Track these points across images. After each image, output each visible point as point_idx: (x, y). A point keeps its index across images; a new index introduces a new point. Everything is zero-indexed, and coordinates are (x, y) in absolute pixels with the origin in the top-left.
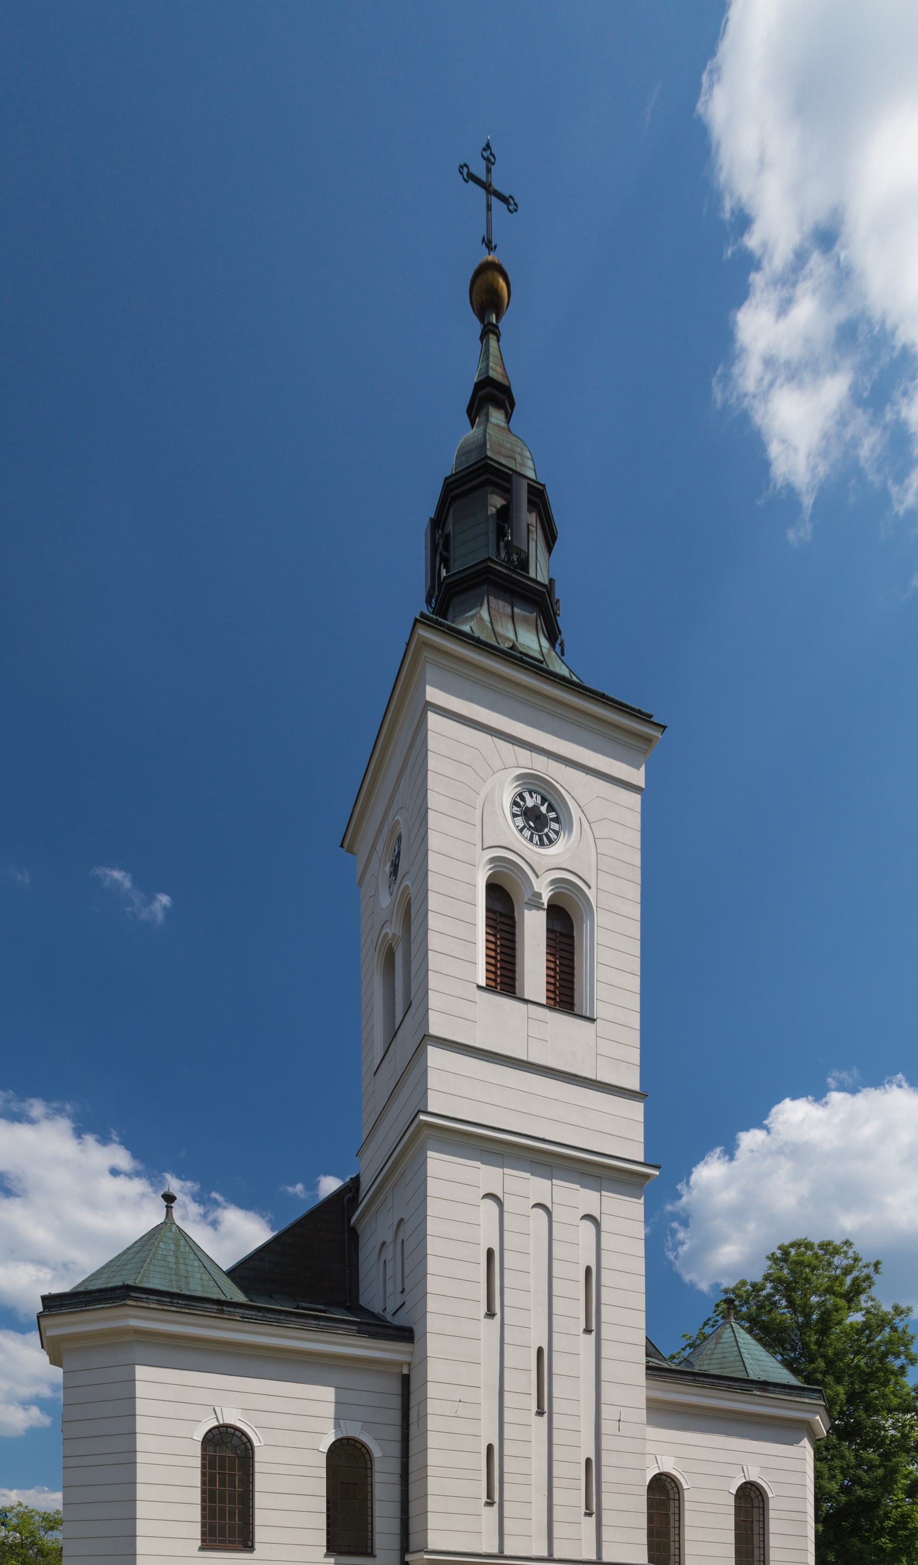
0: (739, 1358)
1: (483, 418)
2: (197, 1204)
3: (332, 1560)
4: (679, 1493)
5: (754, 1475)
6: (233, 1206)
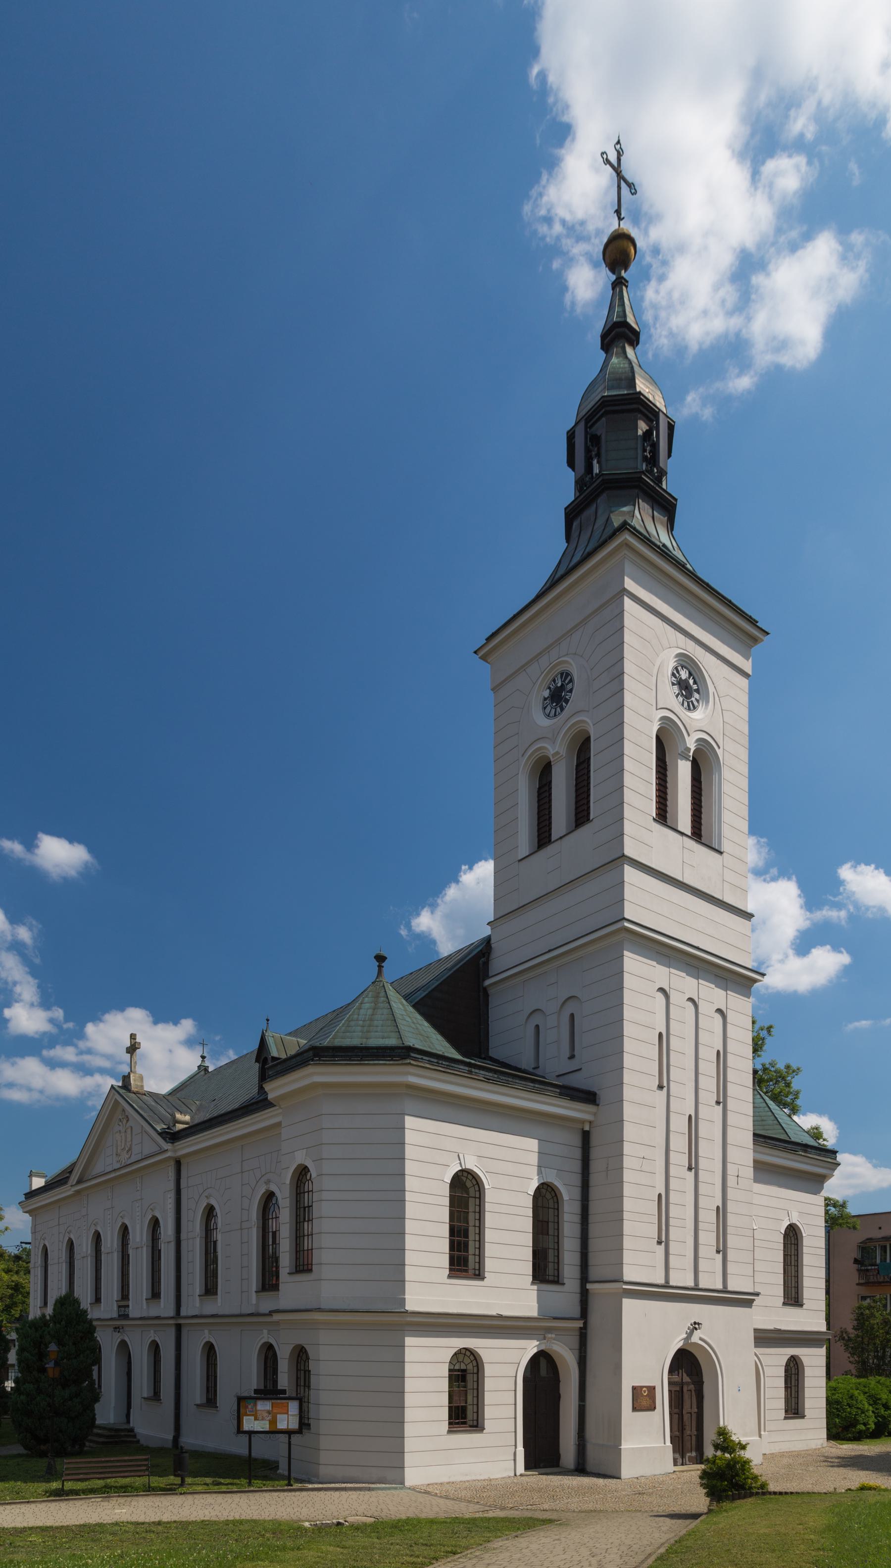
1: (620, 350)
3: (535, 1287)
4: (479, 1190)
5: (471, 1164)
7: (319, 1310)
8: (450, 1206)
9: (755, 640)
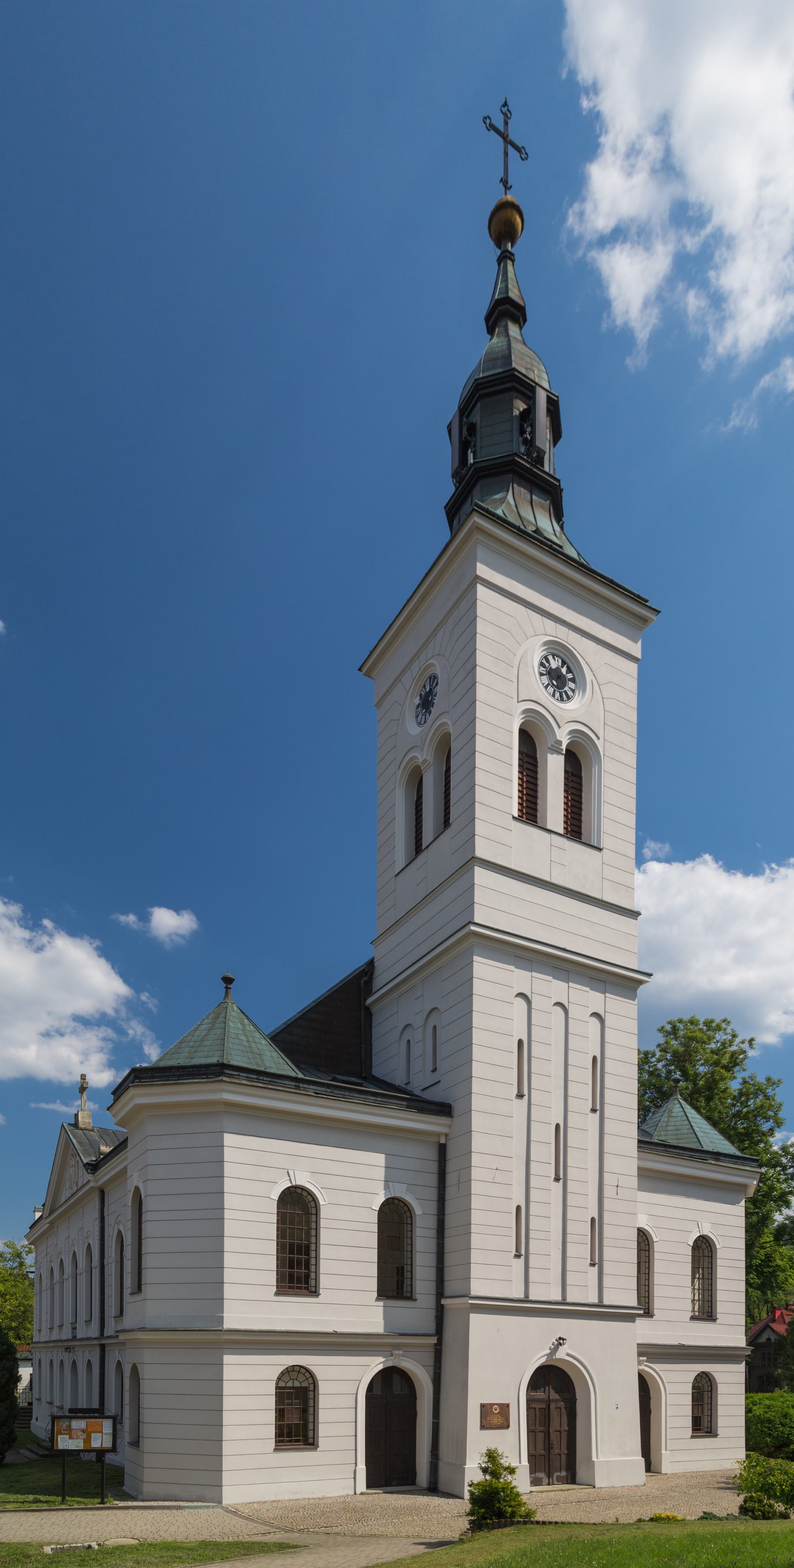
0: (691, 1131)
1: (502, 329)
2: (23, 929)
3: (381, 1303)
5: (706, 1231)
6: (62, 933)
7: (143, 1329)
8: (278, 1223)
9: (645, 620)
